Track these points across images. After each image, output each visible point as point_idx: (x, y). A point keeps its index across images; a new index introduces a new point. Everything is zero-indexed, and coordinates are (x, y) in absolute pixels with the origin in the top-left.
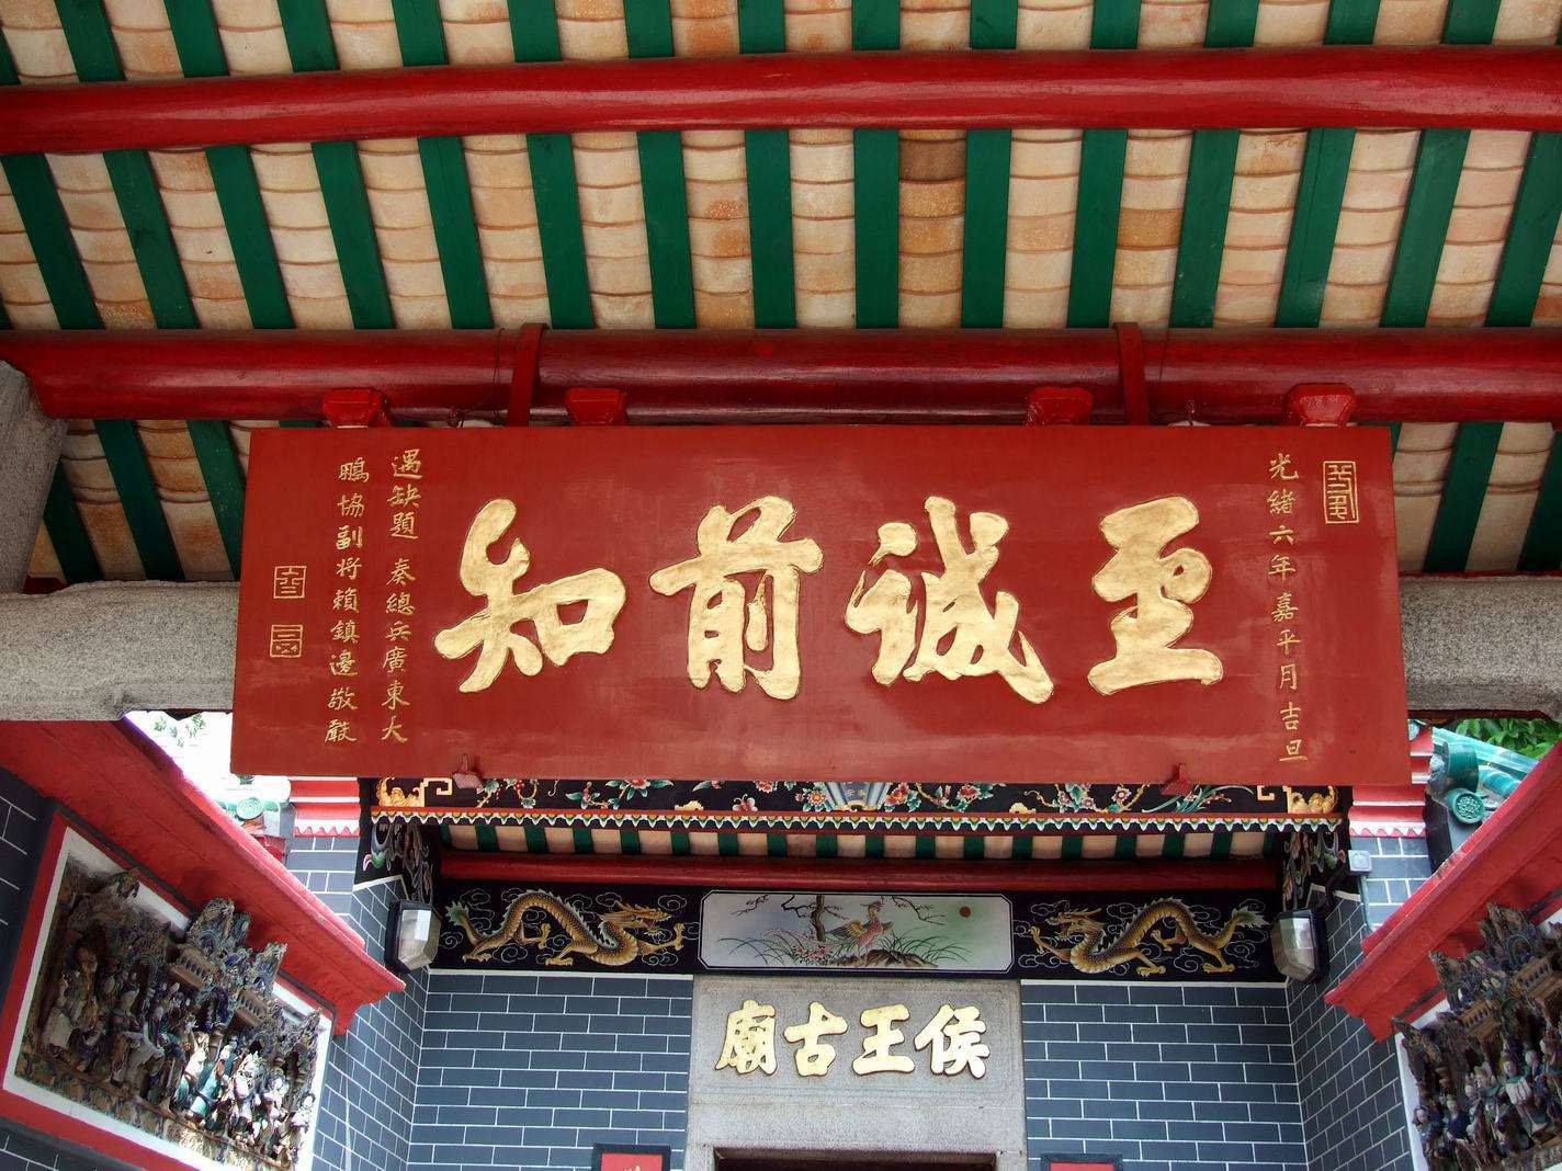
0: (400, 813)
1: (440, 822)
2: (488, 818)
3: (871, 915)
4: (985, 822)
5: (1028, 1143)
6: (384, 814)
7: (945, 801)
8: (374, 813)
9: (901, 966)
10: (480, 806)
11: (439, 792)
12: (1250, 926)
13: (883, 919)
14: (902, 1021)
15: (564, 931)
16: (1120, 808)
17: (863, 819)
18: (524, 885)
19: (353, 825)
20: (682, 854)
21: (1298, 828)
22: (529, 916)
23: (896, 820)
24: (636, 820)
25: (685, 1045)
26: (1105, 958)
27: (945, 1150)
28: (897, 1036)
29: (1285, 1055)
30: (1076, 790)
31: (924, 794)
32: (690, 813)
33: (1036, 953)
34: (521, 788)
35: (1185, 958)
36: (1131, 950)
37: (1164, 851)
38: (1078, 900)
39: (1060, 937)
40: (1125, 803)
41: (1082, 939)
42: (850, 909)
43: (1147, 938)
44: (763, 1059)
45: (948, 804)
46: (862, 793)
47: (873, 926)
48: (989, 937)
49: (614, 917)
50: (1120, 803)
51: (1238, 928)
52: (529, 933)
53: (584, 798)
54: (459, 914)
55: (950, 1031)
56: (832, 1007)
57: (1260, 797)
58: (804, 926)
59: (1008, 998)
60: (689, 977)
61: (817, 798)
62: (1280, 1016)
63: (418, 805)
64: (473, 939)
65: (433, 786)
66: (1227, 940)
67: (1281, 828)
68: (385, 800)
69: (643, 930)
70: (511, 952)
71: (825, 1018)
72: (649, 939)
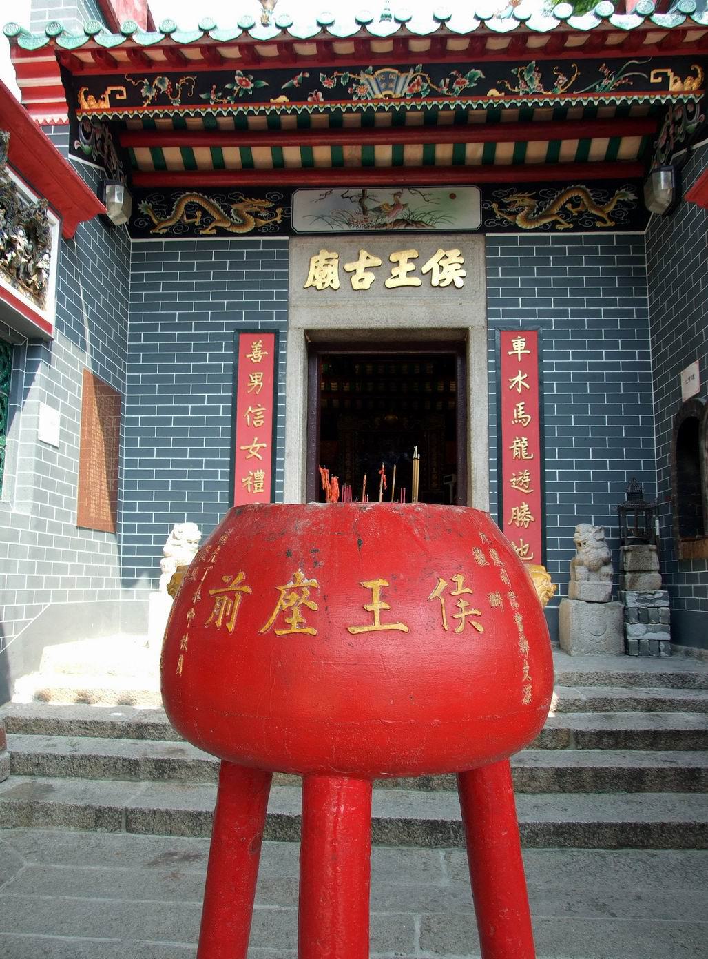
0: (95, 113)
1: (121, 118)
2: (151, 113)
3: (395, 200)
4: (471, 103)
5: (487, 322)
6: (84, 114)
7: (445, 89)
8: (78, 114)
9: (414, 228)
10: (145, 105)
11: (118, 97)
12: (626, 200)
13: (402, 201)
14: (414, 258)
15: (210, 215)
16: (560, 91)
17: (392, 104)
18: (184, 190)
19: (65, 117)
20: (279, 166)
21: (674, 101)
22: (188, 207)
23: (414, 103)
24: (246, 110)
25: (286, 275)
26: (537, 220)
27: (439, 327)
28: (411, 267)
29: (642, 271)
30: (531, 79)
31: (432, 85)
32: (280, 104)
33: (496, 219)
34: (171, 92)
35: (585, 219)
36: (552, 215)
37: (576, 158)
38: (522, 188)
39: (510, 209)
40: (563, 87)
41: (524, 210)
42: (384, 196)
43: (563, 208)
44: (332, 281)
45: (447, 92)
46: (392, 86)
47: (396, 206)
48: (468, 209)
49: (240, 206)
50: (559, 87)
51: (618, 201)
52: (189, 217)
53: (212, 97)
54: (146, 208)
55: (442, 263)
56: (372, 252)
57: (652, 80)
58: (354, 207)
59: (478, 246)
60: (286, 238)
61: (362, 90)
62: (641, 250)
63: (106, 107)
64: (155, 221)
65: (114, 93)
66: (612, 207)
67: (663, 102)
68: (85, 105)
69: (257, 213)
70: (180, 228)
71: (368, 258)
72: (262, 218)
